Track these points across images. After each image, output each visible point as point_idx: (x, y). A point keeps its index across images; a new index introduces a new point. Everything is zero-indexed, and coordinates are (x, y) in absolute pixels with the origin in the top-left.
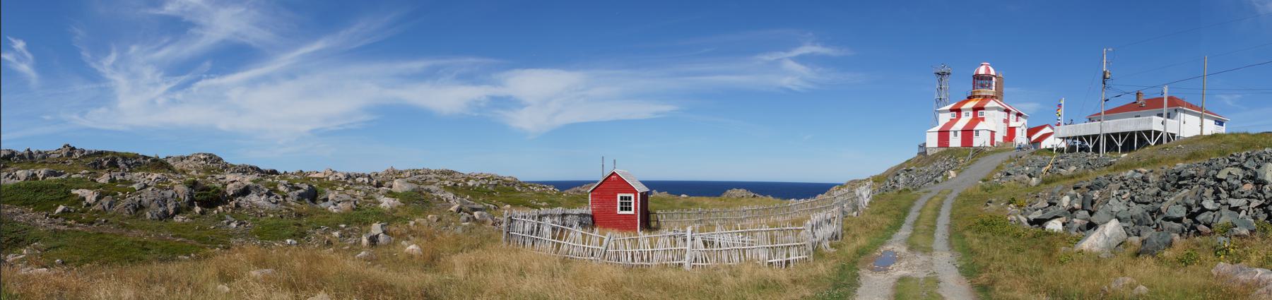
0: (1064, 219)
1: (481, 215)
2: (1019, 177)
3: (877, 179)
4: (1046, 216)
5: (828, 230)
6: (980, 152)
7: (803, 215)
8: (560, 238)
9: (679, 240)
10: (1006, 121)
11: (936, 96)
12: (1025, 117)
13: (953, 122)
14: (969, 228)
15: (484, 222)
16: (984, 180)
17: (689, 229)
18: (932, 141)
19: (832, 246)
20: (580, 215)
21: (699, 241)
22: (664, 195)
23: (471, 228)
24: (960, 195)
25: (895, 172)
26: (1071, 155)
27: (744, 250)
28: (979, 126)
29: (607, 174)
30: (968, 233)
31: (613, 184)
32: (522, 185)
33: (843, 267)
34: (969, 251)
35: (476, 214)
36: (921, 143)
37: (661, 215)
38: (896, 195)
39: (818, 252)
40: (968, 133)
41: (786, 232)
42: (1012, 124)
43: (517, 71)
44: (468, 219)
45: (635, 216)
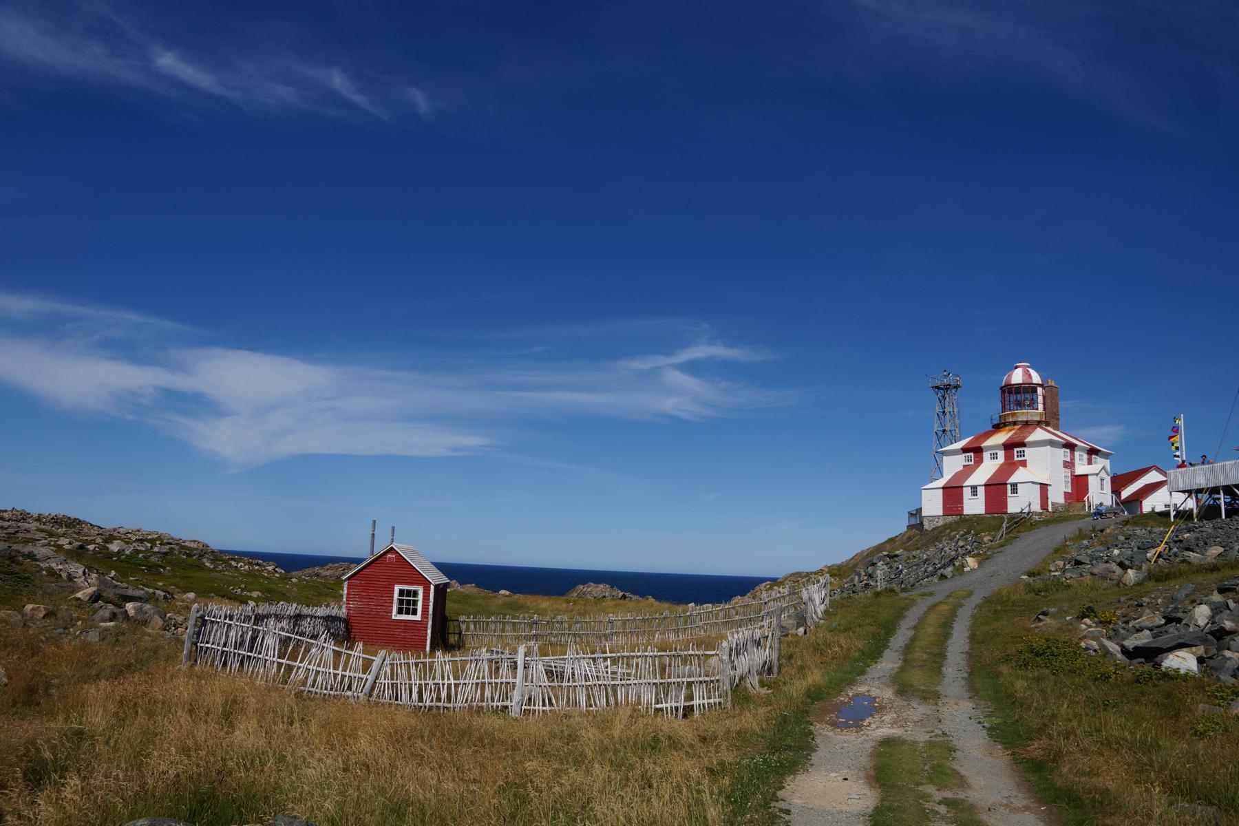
0: (1201, 650)
1: (139, 610)
2: (1100, 568)
3: (836, 572)
4: (1161, 642)
5: (755, 658)
6: (1021, 522)
7: (713, 632)
8: (293, 657)
9: (504, 670)
10: (1069, 465)
11: (937, 427)
12: (1106, 456)
14: (1007, 659)
15: (145, 623)
16: (1030, 574)
17: (521, 650)
18: (932, 505)
19: (762, 684)
20: (328, 618)
21: (539, 669)
22: (470, 589)
23: (119, 633)
24: (988, 601)
25: (868, 559)
26: (1208, 526)
27: (614, 688)
28: (1019, 476)
29: (380, 549)
30: (1004, 669)
31: (388, 568)
32: (218, 556)
33: (785, 719)
34: (1004, 700)
35: (130, 607)
36: (913, 508)
37: (466, 623)
38: (873, 598)
39: (739, 692)
40: (997, 489)
41: (685, 660)
42: (1081, 469)
43: (216, 351)
44: (113, 617)
45: (421, 625)
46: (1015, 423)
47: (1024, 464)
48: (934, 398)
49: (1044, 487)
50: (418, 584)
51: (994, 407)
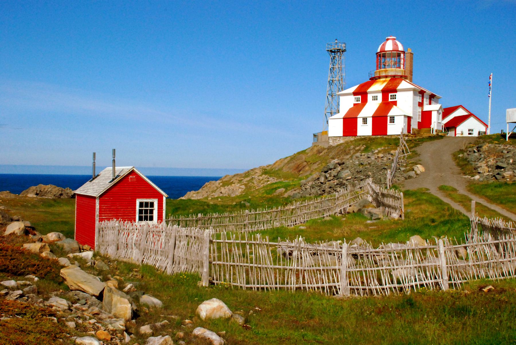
6: (395, 141)
13: (357, 108)
18: (335, 128)
40: (380, 121)
42: (427, 108)
46: (386, 77)
47: (395, 103)
48: (329, 57)
49: (409, 118)
50: (154, 197)
51: (370, 68)
